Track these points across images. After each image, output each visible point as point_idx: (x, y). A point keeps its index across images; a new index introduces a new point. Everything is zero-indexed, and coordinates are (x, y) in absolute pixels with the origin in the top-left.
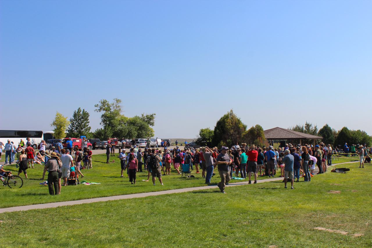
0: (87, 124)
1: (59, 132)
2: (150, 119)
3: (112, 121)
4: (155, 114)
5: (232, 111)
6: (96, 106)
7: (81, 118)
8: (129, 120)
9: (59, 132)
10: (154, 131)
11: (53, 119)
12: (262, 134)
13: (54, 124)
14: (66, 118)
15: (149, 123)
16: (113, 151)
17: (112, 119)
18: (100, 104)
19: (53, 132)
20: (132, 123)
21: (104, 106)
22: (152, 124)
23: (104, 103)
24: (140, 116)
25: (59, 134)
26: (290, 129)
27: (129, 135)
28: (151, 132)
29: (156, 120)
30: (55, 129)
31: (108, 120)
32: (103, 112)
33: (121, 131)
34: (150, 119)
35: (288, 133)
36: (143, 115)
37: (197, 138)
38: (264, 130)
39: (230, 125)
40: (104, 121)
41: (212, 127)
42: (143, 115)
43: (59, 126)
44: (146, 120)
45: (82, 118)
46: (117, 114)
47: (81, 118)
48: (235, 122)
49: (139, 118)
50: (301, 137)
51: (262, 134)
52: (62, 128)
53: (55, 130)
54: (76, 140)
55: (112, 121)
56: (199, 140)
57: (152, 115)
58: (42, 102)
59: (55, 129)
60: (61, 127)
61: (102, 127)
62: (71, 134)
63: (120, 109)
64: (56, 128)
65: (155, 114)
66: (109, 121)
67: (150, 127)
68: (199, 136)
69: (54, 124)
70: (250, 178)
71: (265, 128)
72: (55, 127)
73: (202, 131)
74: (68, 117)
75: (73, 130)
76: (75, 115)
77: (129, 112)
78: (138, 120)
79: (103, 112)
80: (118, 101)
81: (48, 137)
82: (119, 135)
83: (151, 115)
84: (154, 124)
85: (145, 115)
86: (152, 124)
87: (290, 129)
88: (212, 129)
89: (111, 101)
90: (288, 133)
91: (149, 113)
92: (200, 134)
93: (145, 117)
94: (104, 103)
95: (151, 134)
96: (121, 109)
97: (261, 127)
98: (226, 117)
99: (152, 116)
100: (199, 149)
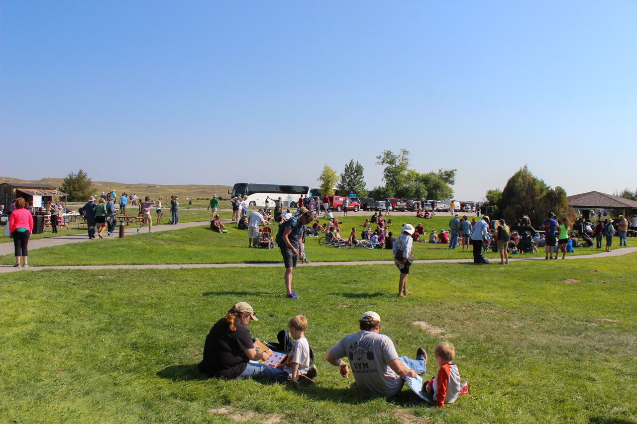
0: (361, 180)
1: (326, 187)
2: (448, 176)
3: (396, 177)
4: (456, 170)
5: (525, 167)
6: (377, 157)
7: (354, 172)
8: (422, 176)
9: (326, 187)
10: (454, 191)
11: (320, 172)
12: (563, 200)
13: (321, 178)
14: (335, 173)
15: (446, 180)
16: (175, 218)
17: (397, 175)
18: (383, 156)
19: (319, 188)
20: (425, 180)
21: (389, 158)
22: (452, 182)
23: (388, 154)
24: (437, 172)
25: (326, 191)
26: (617, 195)
27: (418, 195)
28: (451, 192)
29: (456, 178)
30: (322, 185)
31: (392, 175)
32: (386, 165)
33: (407, 190)
34: (448, 176)
35: (607, 200)
36: (440, 171)
37: (484, 202)
38: (568, 195)
39: (521, 186)
40: (387, 176)
41: (501, 187)
42: (440, 171)
43: (327, 180)
44: (444, 177)
45: (356, 171)
46: (402, 168)
47: (354, 172)
48: (529, 182)
49: (434, 174)
50: (624, 206)
51: (563, 200)
52: (330, 184)
53: (322, 186)
54: (339, 198)
55: (396, 177)
56: (485, 204)
57: (453, 171)
58: (31, 158)
59: (322, 185)
60: (329, 182)
61: (383, 184)
62: (341, 192)
63: (407, 163)
64: (323, 183)
65: (456, 170)
66: (393, 176)
67: (450, 186)
68: (486, 200)
69: (321, 178)
70: (557, 255)
71: (569, 194)
72: (321, 183)
73: (490, 192)
74: (339, 171)
75: (345, 186)
76: (346, 170)
77: (422, 164)
78: (433, 176)
79: (386, 165)
80: (405, 152)
81: (315, 192)
82: (402, 194)
83: (451, 170)
84: (454, 183)
85: (443, 171)
86: (452, 182)
87: (617, 195)
88: (502, 190)
89: (396, 152)
90: (607, 200)
91: (449, 169)
92: (487, 197)
93: (444, 174)
94: (388, 154)
95: (450, 195)
96: (409, 163)
97: (564, 190)
98: (518, 175)
99: (452, 172)
100: (23, 230)
